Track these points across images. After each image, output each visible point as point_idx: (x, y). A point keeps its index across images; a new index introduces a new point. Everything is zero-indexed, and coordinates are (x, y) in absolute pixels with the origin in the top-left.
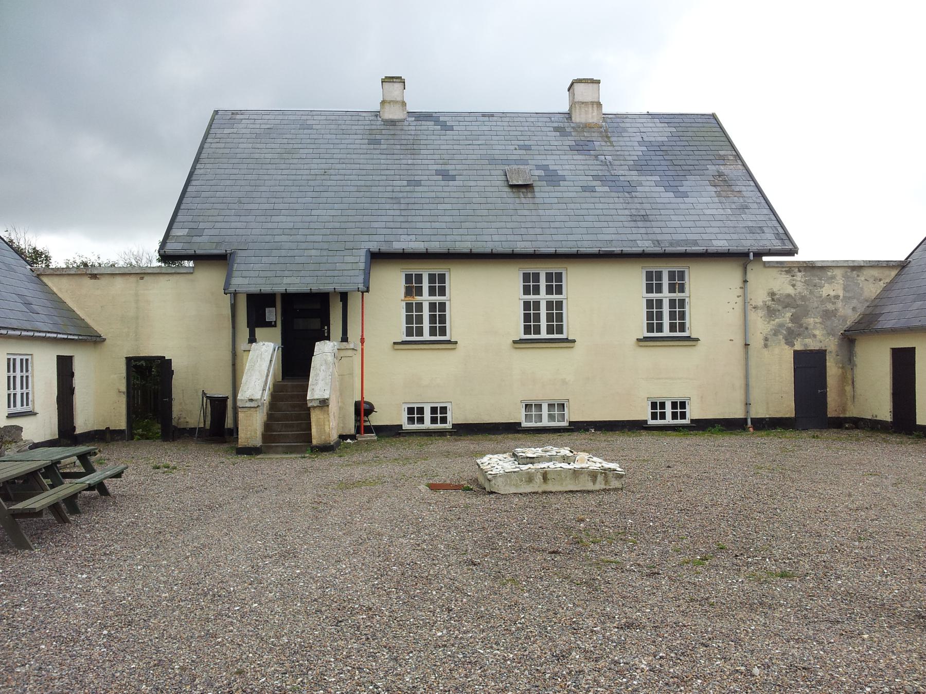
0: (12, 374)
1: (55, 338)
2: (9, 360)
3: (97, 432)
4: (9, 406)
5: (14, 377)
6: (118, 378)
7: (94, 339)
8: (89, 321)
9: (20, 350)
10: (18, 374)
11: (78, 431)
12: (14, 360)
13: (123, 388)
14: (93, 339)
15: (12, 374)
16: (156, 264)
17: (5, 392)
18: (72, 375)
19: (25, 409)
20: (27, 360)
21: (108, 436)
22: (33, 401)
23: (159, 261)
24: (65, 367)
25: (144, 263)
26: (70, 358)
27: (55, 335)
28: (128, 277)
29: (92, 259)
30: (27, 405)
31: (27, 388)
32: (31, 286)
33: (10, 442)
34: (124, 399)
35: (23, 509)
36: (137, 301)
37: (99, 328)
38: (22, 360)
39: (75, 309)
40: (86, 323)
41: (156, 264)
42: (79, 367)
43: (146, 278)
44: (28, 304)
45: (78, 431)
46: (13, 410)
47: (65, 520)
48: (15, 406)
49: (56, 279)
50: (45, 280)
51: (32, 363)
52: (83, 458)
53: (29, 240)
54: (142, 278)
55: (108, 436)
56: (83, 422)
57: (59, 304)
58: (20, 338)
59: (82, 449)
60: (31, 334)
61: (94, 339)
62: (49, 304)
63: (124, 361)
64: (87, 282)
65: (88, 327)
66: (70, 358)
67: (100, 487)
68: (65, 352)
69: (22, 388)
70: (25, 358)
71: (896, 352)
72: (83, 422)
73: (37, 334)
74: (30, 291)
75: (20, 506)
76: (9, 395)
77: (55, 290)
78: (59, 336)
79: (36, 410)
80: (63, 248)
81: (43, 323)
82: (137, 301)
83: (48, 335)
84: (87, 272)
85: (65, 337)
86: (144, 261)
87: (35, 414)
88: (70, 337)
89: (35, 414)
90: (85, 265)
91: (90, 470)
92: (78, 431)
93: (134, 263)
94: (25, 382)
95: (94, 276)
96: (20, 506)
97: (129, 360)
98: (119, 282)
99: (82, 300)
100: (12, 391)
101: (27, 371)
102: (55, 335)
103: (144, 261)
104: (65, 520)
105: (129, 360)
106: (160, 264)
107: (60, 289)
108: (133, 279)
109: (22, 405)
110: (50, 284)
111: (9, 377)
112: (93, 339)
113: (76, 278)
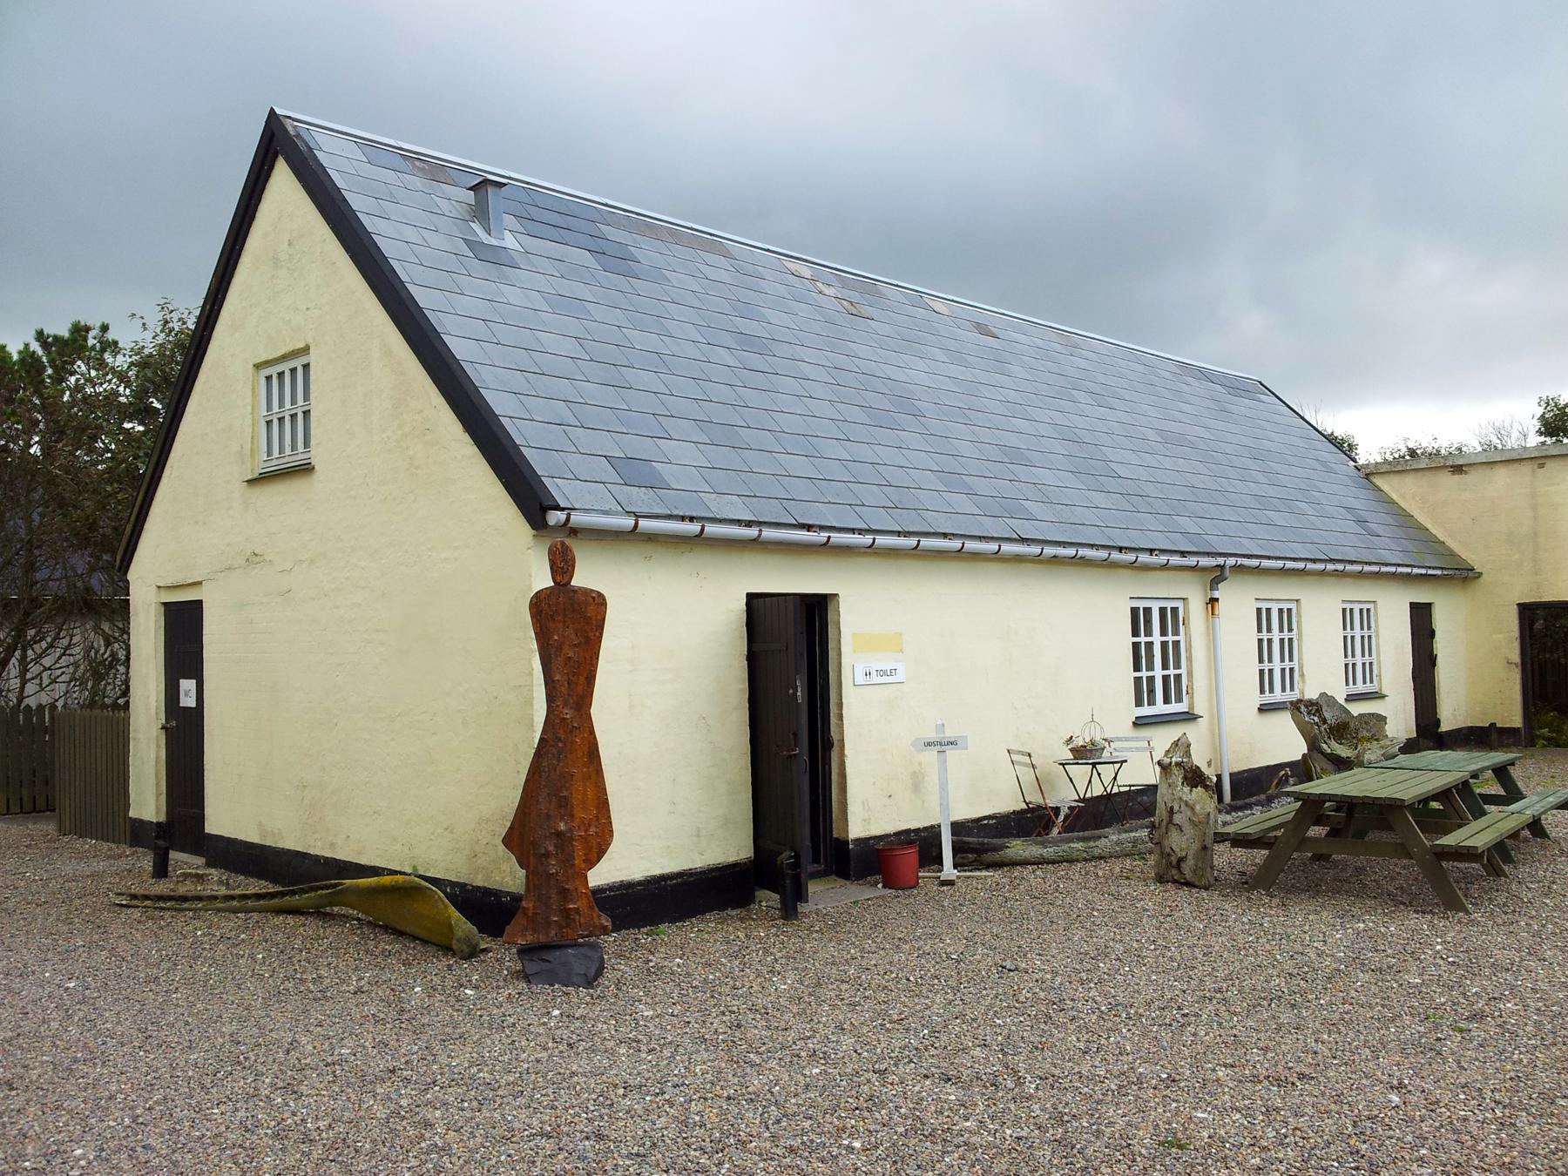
0: (1349, 633)
1: (1409, 574)
2: (1259, 610)
3: (1471, 731)
4: (1262, 692)
5: (1270, 641)
6: (1506, 639)
7: (1465, 574)
8: (1452, 544)
9: (1361, 593)
10: (1357, 633)
11: (1444, 728)
12: (1269, 610)
13: (1516, 656)
14: (1461, 575)
15: (1265, 635)
16: (1534, 440)
17: (1255, 667)
18: (1432, 634)
19: (1368, 688)
20: (1289, 610)
21: (1494, 737)
22: (1379, 676)
23: (1541, 433)
24: (1421, 618)
25: (1513, 442)
26: (1427, 607)
27: (1408, 570)
28: (1515, 465)
29: (1423, 439)
30: (1292, 689)
31: (1291, 660)
32: (1361, 493)
33: (1368, 740)
34: (1516, 676)
35: (1458, 847)
36: (1534, 507)
37: (1471, 556)
38: (1281, 611)
39: (1429, 526)
40: (1448, 548)
41: (1534, 440)
42: (1440, 621)
43: (1549, 464)
44: (1361, 522)
45: (1445, 727)
46: (1268, 698)
47: (1498, 873)
48: (1271, 691)
49: (1395, 479)
50: (1378, 481)
51: (1376, 614)
52: (1501, 772)
53: (1335, 422)
54: (1542, 466)
55: (1494, 737)
56: (1451, 715)
57: (1404, 520)
58: (1361, 575)
59: (1499, 757)
60: (1375, 568)
61: (1465, 574)
62: (1389, 520)
63: (1514, 611)
64: (1449, 480)
65: (1452, 554)
66: (1427, 607)
67: (1536, 827)
68: (1422, 598)
69: (1282, 660)
70: (1365, 607)
71: (1414, 607)
72: (1451, 715)
73: (1384, 569)
74: (1359, 499)
75: (1449, 840)
76: (1261, 672)
77: (1395, 497)
78: (1416, 571)
79: (1384, 692)
80: (1377, 428)
81: (1389, 551)
82: (1534, 507)
83: (1400, 570)
84: (1413, 462)
85: (1423, 571)
86: (1515, 434)
87: (1383, 697)
88: (1430, 572)
89: (1383, 697)
90: (1412, 453)
91: (1513, 794)
92: (1444, 728)
93: (1495, 441)
94: (1367, 643)
95: (1458, 469)
96: (1449, 840)
97: (1528, 612)
98: (1501, 476)
99: (1437, 508)
100: (1266, 666)
101: (1290, 630)
102: (1408, 570)
103: (1515, 434)
104: (1498, 873)
105: (1528, 612)
106: (1542, 439)
107: (1403, 496)
108: (1525, 469)
109: (1283, 690)
110: (1386, 488)
111: (1260, 641)
112: (1461, 575)
113: (1427, 473)
